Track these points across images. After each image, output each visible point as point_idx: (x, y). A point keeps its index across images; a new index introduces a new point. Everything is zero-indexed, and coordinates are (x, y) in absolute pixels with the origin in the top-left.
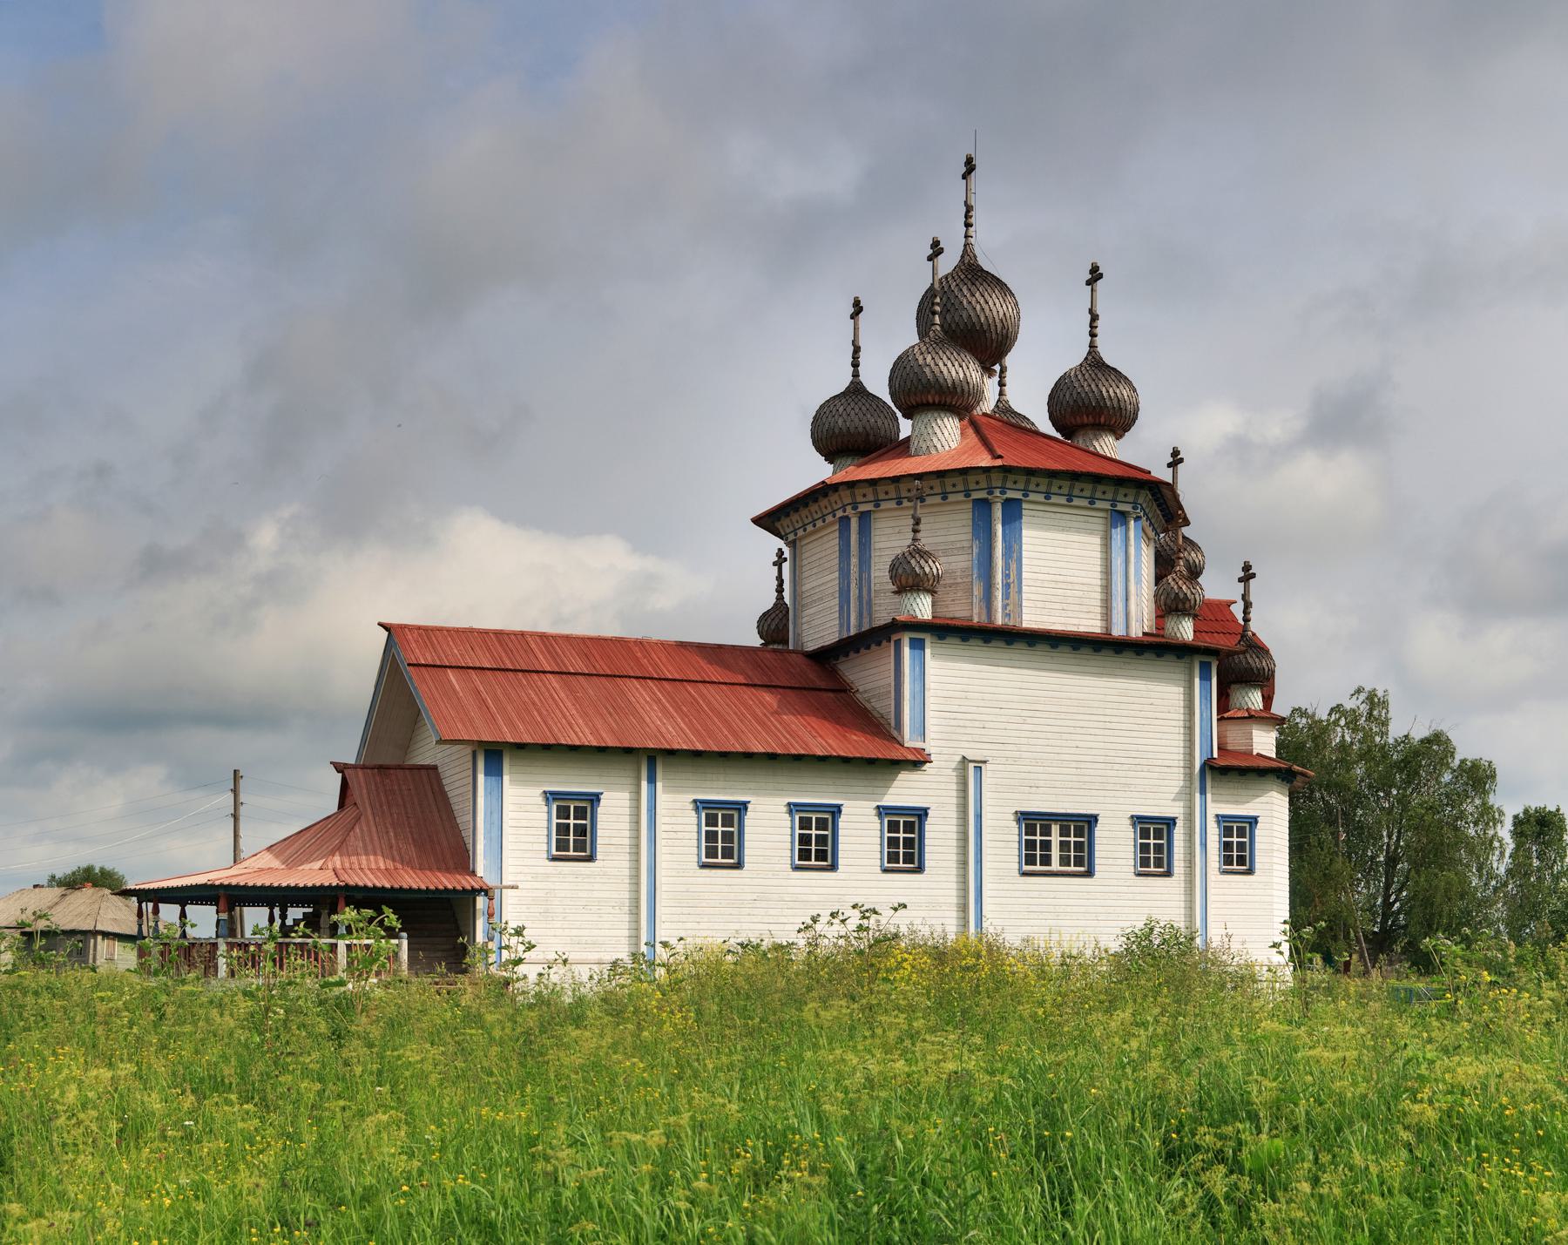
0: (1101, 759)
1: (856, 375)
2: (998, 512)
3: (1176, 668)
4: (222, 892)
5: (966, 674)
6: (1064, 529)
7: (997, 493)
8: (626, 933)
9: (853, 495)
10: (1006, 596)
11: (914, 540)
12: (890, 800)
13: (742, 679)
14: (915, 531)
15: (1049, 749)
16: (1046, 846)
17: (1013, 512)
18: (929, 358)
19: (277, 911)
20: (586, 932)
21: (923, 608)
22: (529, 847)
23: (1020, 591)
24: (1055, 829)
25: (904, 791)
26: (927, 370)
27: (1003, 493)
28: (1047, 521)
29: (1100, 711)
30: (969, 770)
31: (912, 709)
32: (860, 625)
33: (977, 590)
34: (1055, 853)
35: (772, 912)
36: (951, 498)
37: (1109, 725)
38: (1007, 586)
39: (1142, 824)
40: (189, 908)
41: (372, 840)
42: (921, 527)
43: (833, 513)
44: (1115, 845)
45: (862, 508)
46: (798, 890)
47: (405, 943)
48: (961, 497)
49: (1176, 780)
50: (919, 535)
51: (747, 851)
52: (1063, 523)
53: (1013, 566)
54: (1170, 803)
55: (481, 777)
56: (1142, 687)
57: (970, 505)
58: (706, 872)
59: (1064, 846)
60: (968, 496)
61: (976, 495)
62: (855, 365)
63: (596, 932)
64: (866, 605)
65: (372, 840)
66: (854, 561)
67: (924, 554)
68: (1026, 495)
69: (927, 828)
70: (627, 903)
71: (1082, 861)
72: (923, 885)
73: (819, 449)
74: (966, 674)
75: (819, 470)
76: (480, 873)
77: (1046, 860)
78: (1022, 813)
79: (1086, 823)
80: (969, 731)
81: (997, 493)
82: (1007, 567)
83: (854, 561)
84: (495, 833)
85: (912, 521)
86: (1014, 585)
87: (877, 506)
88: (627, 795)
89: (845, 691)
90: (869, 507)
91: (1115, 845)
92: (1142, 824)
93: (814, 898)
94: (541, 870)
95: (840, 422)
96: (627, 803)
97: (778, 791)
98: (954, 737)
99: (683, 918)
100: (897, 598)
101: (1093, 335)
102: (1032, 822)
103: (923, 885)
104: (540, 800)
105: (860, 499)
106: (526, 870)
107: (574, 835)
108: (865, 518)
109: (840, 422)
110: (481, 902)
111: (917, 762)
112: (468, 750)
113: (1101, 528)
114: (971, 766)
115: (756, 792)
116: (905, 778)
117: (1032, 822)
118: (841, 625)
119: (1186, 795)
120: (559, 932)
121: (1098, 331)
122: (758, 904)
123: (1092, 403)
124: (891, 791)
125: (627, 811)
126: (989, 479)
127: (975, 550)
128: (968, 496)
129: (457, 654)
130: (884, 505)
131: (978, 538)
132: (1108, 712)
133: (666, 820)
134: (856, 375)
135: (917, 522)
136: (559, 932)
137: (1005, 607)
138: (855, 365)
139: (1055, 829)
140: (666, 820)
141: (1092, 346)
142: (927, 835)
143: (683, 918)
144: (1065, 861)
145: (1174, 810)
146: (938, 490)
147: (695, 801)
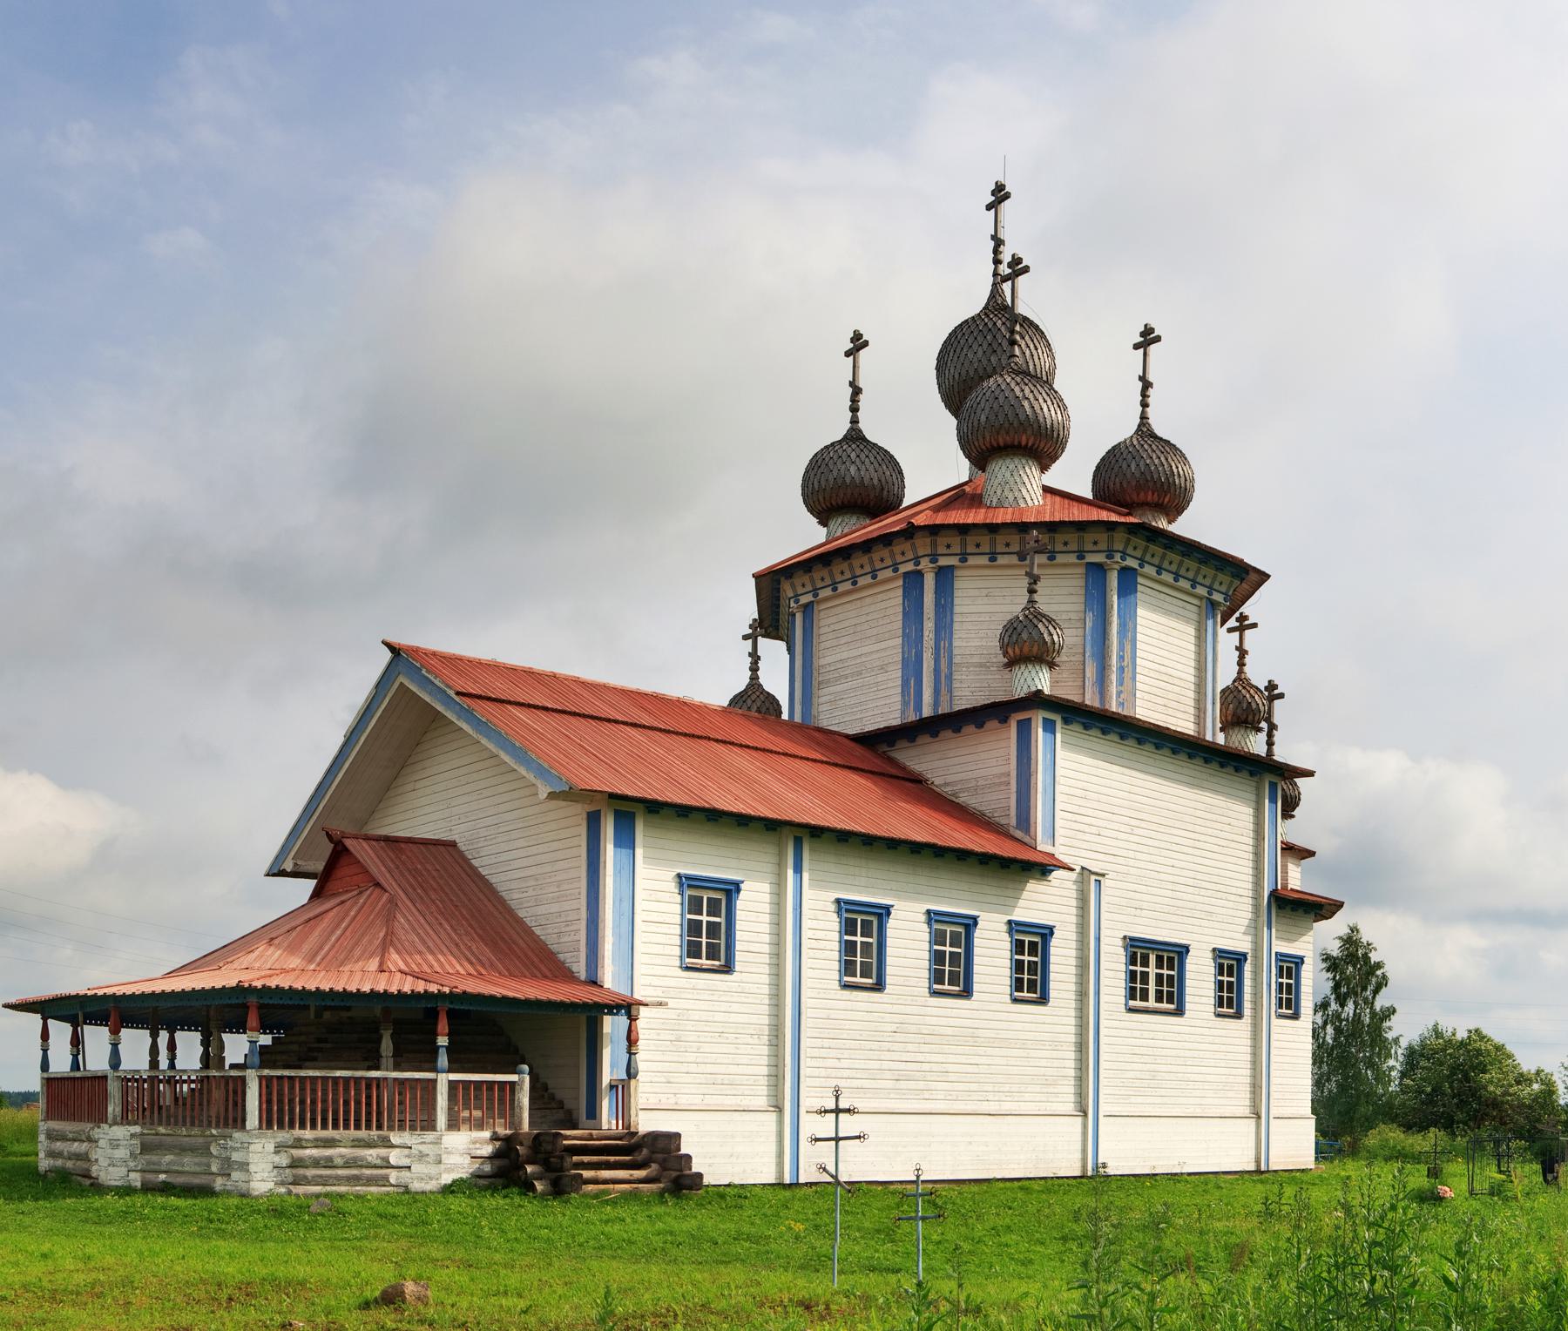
0: (1191, 882)
1: (855, 421)
2: (1113, 579)
3: (1245, 785)
4: (253, 1000)
5: (1085, 769)
6: (1168, 613)
7: (1118, 557)
8: (765, 1071)
9: (934, 545)
10: (1121, 682)
11: (1031, 601)
12: (1020, 915)
13: (818, 756)
14: (1032, 591)
15: (1151, 866)
16: (1145, 975)
17: (1128, 581)
18: (1027, 391)
19: (164, 1036)
20: (722, 1069)
21: (1042, 680)
22: (659, 949)
23: (1134, 679)
24: (1152, 959)
25: (1042, 903)
26: (1026, 404)
27: (1123, 559)
28: (1154, 601)
29: (1190, 827)
30: (1089, 880)
31: (1044, 805)
32: (936, 704)
33: (1091, 671)
34: (1152, 987)
35: (910, 1047)
36: (1060, 559)
37: (1197, 844)
38: (1121, 669)
39: (1219, 954)
40: (50, 1022)
41: (427, 934)
42: (1038, 587)
43: (1124, 555)
44: (1200, 978)
45: (943, 562)
46: (934, 1021)
47: (527, 1078)
48: (1072, 558)
49: (1245, 913)
50: (1036, 597)
51: (889, 970)
52: (1166, 605)
53: (1128, 648)
54: (1241, 936)
55: (609, 850)
56: (1223, 804)
57: (1082, 570)
58: (847, 993)
59: (1159, 977)
60: (1081, 557)
61: (1091, 558)
62: (854, 409)
63: (733, 1069)
64: (943, 680)
65: (427, 934)
66: (929, 626)
67: (1040, 616)
68: (816, 595)
69: (1053, 950)
70: (766, 1030)
71: (1173, 998)
72: (1048, 1019)
73: (811, 510)
74: (1085, 769)
75: (808, 534)
76: (608, 983)
77: (1145, 997)
78: (1132, 939)
79: (1174, 955)
80: (1087, 837)
81: (1118, 557)
82: (1121, 648)
83: (929, 626)
84: (626, 927)
85: (1025, 582)
86: (1128, 671)
87: (964, 560)
88: (766, 887)
89: (920, 782)
90: (953, 561)
91: (1200, 978)
92: (1219, 954)
93: (949, 1031)
94: (672, 982)
95: (853, 469)
96: (767, 898)
97: (917, 895)
98: (1075, 843)
99: (824, 1053)
100: (1006, 673)
101: (1145, 405)
102: (1137, 950)
103: (1048, 1019)
104: (673, 887)
105: (899, 559)
106: (655, 981)
107: (708, 941)
108: (945, 577)
109: (853, 469)
110: (612, 1026)
111: (1041, 868)
112: (578, 812)
113: (1195, 617)
114: (1093, 878)
115: (899, 898)
116: (1033, 888)
117: (1137, 950)
118: (905, 703)
119: (1254, 930)
120: (693, 1068)
121: (1150, 400)
122: (898, 1037)
123: (1143, 483)
124: (1021, 903)
125: (767, 908)
126: (1111, 540)
127: (1089, 624)
128: (1081, 557)
129: (501, 689)
130: (972, 561)
131: (1092, 610)
132: (1198, 829)
133: (814, 924)
134: (855, 421)
135: (1035, 580)
136: (693, 1068)
137: (1119, 693)
138: (854, 409)
139: (1152, 959)
140: (814, 924)
141: (1144, 417)
142: (1052, 959)
143: (824, 1053)
144: (1159, 999)
145: (1242, 944)
146: (1015, 548)
147: (838, 901)
